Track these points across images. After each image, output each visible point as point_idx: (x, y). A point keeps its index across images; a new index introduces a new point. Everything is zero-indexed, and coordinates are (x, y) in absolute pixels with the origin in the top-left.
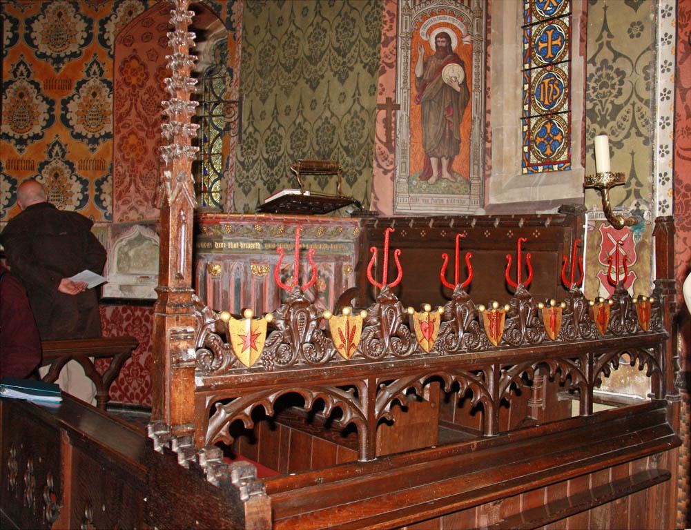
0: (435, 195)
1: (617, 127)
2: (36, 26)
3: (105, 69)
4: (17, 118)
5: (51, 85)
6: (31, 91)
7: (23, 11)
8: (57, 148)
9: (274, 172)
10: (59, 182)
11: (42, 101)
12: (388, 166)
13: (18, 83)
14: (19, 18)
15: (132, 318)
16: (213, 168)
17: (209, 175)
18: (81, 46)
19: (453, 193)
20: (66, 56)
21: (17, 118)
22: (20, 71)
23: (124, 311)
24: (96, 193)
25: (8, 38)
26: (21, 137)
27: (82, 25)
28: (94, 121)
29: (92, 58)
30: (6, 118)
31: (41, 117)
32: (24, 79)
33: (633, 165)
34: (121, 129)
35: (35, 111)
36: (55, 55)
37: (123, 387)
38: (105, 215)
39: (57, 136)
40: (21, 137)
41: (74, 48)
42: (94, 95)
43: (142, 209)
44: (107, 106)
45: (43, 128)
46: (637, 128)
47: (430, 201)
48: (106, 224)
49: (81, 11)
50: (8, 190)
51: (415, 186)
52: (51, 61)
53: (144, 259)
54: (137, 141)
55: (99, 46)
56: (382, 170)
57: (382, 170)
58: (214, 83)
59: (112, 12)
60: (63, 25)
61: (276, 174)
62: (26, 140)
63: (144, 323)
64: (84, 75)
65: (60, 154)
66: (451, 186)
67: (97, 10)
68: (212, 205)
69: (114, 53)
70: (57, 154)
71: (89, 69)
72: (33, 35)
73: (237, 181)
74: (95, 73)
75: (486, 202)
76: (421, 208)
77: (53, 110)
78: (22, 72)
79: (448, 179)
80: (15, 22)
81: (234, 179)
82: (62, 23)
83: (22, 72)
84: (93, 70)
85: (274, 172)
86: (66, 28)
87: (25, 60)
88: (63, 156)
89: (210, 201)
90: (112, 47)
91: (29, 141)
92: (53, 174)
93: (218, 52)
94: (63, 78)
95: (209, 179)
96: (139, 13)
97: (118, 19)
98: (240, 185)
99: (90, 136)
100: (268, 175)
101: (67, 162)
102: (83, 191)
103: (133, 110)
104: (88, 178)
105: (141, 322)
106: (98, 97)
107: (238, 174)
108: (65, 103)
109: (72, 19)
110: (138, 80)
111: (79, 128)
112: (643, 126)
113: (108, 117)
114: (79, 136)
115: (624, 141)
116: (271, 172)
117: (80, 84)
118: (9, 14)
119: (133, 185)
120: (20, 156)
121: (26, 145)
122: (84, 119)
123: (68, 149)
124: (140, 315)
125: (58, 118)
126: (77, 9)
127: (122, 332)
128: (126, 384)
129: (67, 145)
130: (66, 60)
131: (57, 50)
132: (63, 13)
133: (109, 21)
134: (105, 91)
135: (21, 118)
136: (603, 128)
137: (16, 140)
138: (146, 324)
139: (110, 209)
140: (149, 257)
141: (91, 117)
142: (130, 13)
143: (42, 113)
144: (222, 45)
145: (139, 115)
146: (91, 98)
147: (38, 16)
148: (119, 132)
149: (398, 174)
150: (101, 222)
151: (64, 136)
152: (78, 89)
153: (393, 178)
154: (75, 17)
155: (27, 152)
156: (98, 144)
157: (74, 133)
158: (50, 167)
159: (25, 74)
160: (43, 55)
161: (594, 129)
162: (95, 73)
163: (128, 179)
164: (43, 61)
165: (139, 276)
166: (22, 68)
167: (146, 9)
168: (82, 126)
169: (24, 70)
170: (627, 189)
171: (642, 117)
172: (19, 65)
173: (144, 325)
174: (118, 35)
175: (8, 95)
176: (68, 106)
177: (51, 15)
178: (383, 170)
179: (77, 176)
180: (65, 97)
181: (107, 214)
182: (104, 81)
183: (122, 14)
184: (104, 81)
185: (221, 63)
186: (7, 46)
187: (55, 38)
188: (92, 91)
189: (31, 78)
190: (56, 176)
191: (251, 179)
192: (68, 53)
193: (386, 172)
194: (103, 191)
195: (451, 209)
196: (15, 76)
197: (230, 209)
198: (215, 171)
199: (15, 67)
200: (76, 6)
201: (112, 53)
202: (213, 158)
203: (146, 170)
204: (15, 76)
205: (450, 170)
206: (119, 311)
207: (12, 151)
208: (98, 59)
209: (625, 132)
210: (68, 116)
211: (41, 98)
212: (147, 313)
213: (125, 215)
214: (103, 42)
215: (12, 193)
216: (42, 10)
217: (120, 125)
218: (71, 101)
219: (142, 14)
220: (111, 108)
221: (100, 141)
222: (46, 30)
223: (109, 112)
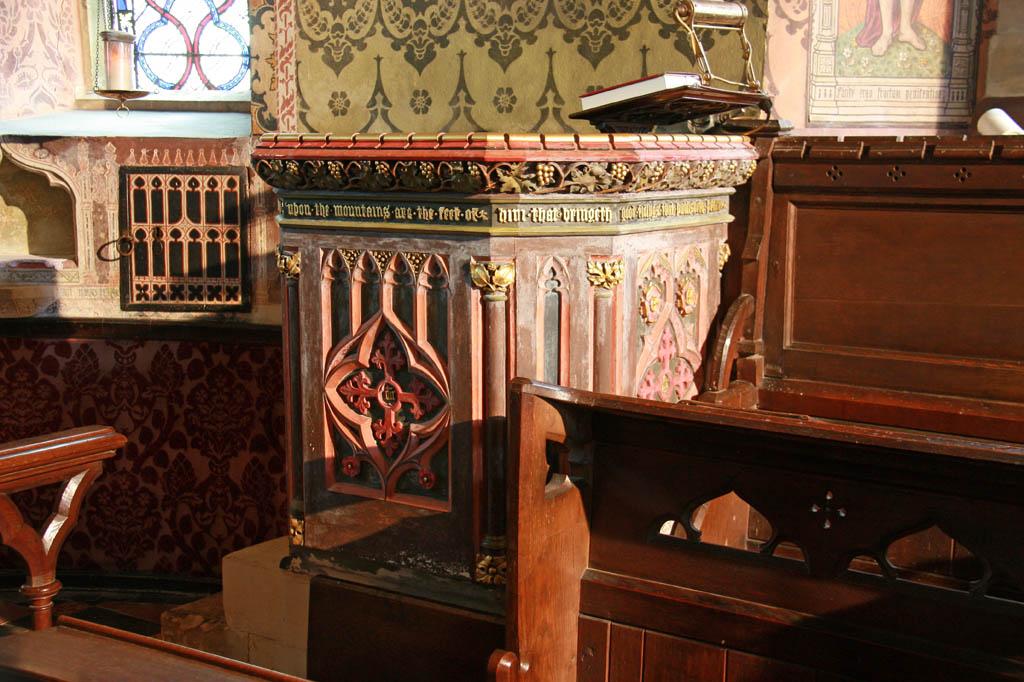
0: (882, 81)
1: (526, 10)
9: (427, 19)
12: (485, 26)
19: (920, 76)
33: (462, 71)
37: (188, 540)
46: (467, 19)
47: (875, 95)
51: (847, 61)
56: (785, 22)
57: (785, 22)
61: (434, 23)
63: (42, 376)
66: (915, 59)
73: (303, 35)
75: (978, 95)
76: (858, 111)
79: (909, 43)
81: (293, 32)
85: (427, 19)
98: (314, 46)
100: (406, 25)
105: (34, 375)
107: (304, 19)
112: (392, 22)
115: (449, 37)
116: (414, 19)
119: (37, 37)
124: (225, 363)
127: (181, 404)
128: (196, 528)
136: (420, 14)
138: (50, 378)
149: (815, 32)
153: (806, 43)
161: (325, 19)
170: (455, 107)
171: (391, 8)
173: (44, 381)
178: (308, 43)
191: (434, 31)
193: (792, 28)
195: (911, 111)
197: (287, 102)
205: (916, 27)
209: (451, 23)
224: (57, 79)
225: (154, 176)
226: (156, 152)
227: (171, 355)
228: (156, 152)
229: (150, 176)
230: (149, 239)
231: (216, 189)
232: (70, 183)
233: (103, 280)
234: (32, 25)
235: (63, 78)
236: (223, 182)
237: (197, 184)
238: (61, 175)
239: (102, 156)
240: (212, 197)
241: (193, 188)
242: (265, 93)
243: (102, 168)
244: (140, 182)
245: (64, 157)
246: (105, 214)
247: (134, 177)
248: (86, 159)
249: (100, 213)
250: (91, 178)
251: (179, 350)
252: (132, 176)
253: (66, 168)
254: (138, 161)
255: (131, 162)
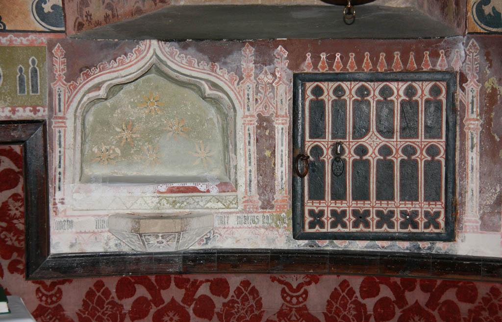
15: (153, 310)
23: (370, 290)
48: (44, 39)
53: (125, 134)
140: (139, 127)
150: (26, 32)
165: (163, 188)
206: (107, 293)
212: (204, 290)
230: (328, 157)
233: (267, 205)
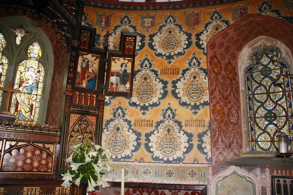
2: (155, 38)
3: (201, 61)
4: (142, 93)
5: (164, 72)
6: (152, 76)
7: (148, 31)
8: (169, 112)
10: (171, 135)
11: (159, 82)
13: (144, 71)
14: (146, 35)
16: (258, 126)
17: (255, 131)
18: (184, 49)
20: (175, 55)
21: (142, 93)
22: (145, 64)
24: (199, 143)
25: (138, 45)
26: (144, 105)
27: (184, 37)
28: (195, 94)
29: (192, 56)
30: (135, 93)
31: (158, 92)
32: (147, 69)
34: (213, 99)
35: (154, 88)
36: (167, 54)
38: (206, 158)
39: (169, 104)
40: (144, 105)
41: (180, 50)
42: (195, 77)
43: (225, 153)
44: (204, 84)
45: (160, 99)
48: (207, 165)
49: (184, 30)
50: (135, 140)
52: (165, 58)
54: (220, 108)
55: (196, 48)
58: (254, 75)
59: (204, 29)
60: (172, 38)
62: (148, 107)
64: (187, 66)
65: (171, 116)
67: (194, 29)
68: (258, 149)
69: (207, 52)
70: (169, 116)
71: (190, 62)
72: (153, 44)
74: (194, 64)
77: (166, 87)
78: (146, 64)
80: (143, 37)
82: (172, 36)
83: (146, 64)
84: (193, 63)
86: (174, 39)
87: (149, 58)
88: (173, 117)
89: (257, 147)
90: (205, 49)
91: (149, 108)
92: (166, 129)
93: (254, 58)
94: (173, 68)
95: (255, 133)
96: (223, 28)
97: (209, 33)
99: (193, 104)
101: (176, 122)
102: (188, 141)
103: (217, 88)
104: (192, 132)
106: (197, 79)
108: (174, 83)
109: (178, 34)
110: (218, 70)
111: (185, 99)
113: (205, 91)
114: (184, 104)
117: (184, 71)
118: (139, 33)
120: (143, 117)
121: (148, 110)
122: (188, 93)
123: (177, 112)
125: (170, 93)
126: (181, 29)
129: (176, 110)
130: (175, 57)
131: (169, 51)
132: (172, 31)
133: (202, 34)
134: (202, 75)
135: (144, 93)
137: (141, 107)
139: (210, 154)
140: (232, 187)
141: (192, 92)
142: (217, 29)
143: (159, 89)
144: (256, 54)
145: (220, 91)
146: (192, 79)
147: (157, 33)
148: (212, 101)
151: (174, 103)
152: (183, 74)
154: (180, 33)
155: (149, 115)
156: (199, 109)
157: (181, 102)
158: (164, 125)
159: (148, 66)
160: (160, 55)
162: (194, 64)
163: (217, 133)
164: (160, 58)
166: (146, 62)
167: (228, 26)
168: (187, 98)
169: (147, 64)
172: (145, 60)
174: (209, 42)
175: (137, 79)
176: (177, 85)
177: (165, 32)
179: (132, 129)
180: (175, 79)
181: (208, 158)
182: (201, 69)
183: (211, 30)
184: (201, 69)
185: (257, 63)
186: (138, 50)
187: (168, 44)
188: (193, 75)
189: (152, 68)
190: (169, 130)
192: (176, 53)
194: (204, 141)
196: (142, 67)
198: (260, 128)
199: (142, 62)
200: (180, 27)
201: (205, 52)
202: (257, 120)
203: (225, 127)
204: (142, 67)
207: (137, 114)
208: (196, 56)
210: (177, 91)
211: (158, 80)
213: (218, 158)
214: (199, 46)
215: (137, 142)
216: (159, 30)
217: (212, 97)
218: (179, 82)
219: (225, 29)
220: (207, 86)
221: (200, 107)
222: (162, 40)
223: (206, 88)
224: (238, 149)
225: (284, 179)
226: (284, 171)
227: (130, 192)
228: (284, 171)
229: (282, 179)
231: (286, 183)
232: (254, 180)
234: (234, 135)
235: (240, 149)
236: (281, 180)
237: (286, 182)
238: (251, 178)
239: (265, 172)
240: (285, 186)
241: (285, 183)
242: (208, 152)
243: (265, 176)
244: (278, 181)
245: (252, 172)
246: (266, 191)
247: (276, 179)
248: (259, 173)
249: (264, 190)
250: (261, 179)
251: (132, 190)
252: (275, 179)
253: (253, 176)
254: (277, 174)
255: (275, 174)
